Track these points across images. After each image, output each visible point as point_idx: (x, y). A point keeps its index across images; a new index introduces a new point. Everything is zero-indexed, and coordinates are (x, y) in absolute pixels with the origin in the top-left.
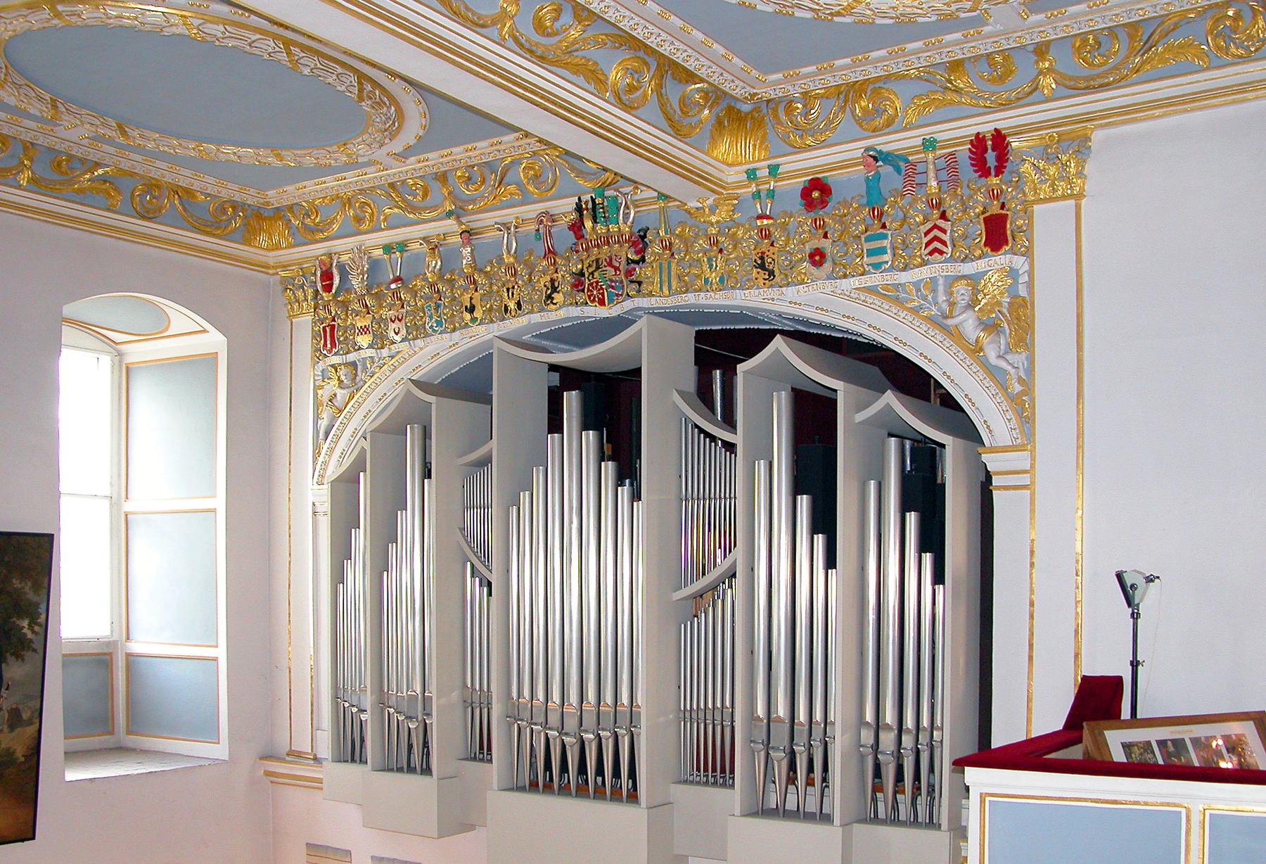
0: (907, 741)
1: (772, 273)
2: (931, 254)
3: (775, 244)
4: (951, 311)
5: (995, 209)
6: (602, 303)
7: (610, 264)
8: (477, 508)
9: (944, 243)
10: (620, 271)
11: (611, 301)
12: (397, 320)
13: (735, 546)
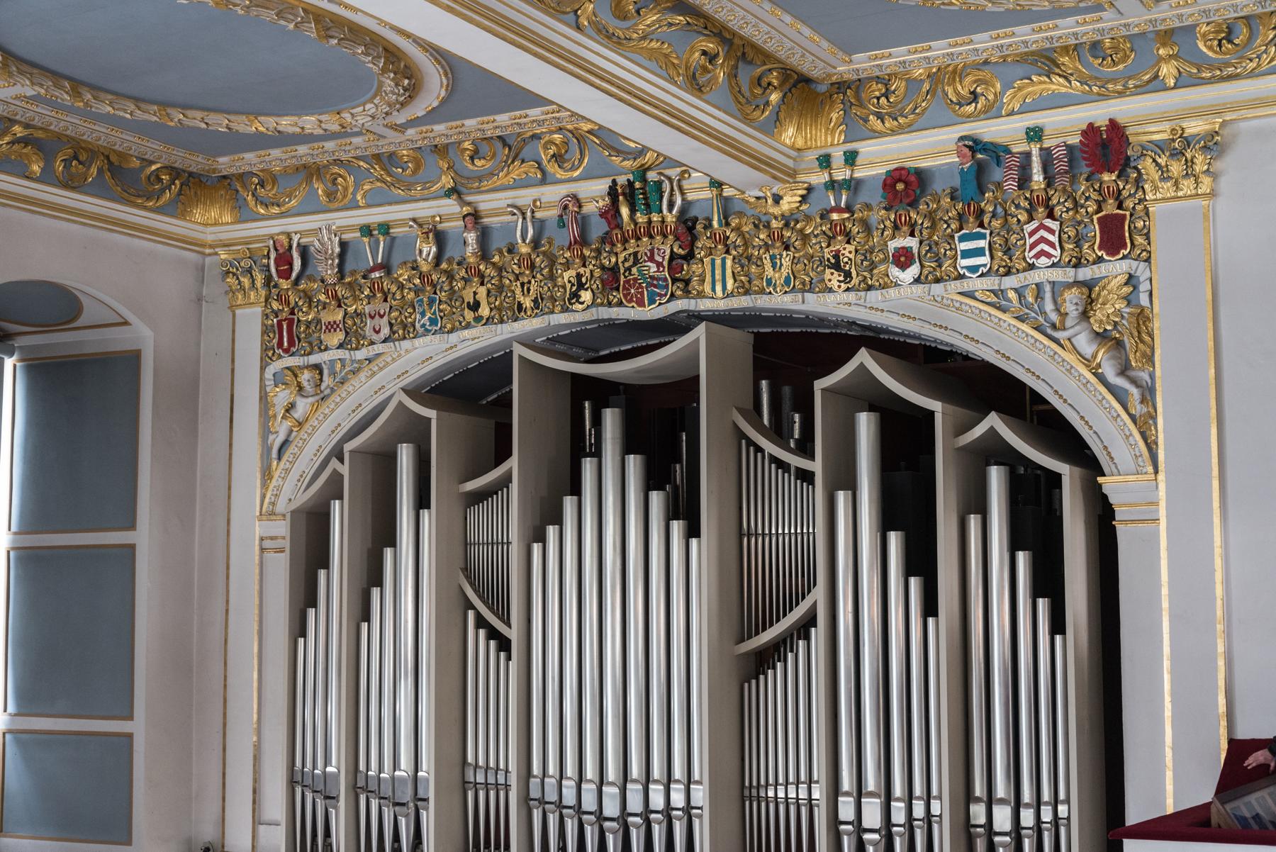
0: (1027, 818)
1: (848, 275)
2: (1037, 256)
3: (851, 241)
4: (1063, 322)
5: (1110, 208)
6: (641, 304)
7: (652, 259)
8: (784, 533)
9: (1052, 245)
10: (664, 267)
11: (652, 302)
12: (377, 316)
13: (815, 585)
